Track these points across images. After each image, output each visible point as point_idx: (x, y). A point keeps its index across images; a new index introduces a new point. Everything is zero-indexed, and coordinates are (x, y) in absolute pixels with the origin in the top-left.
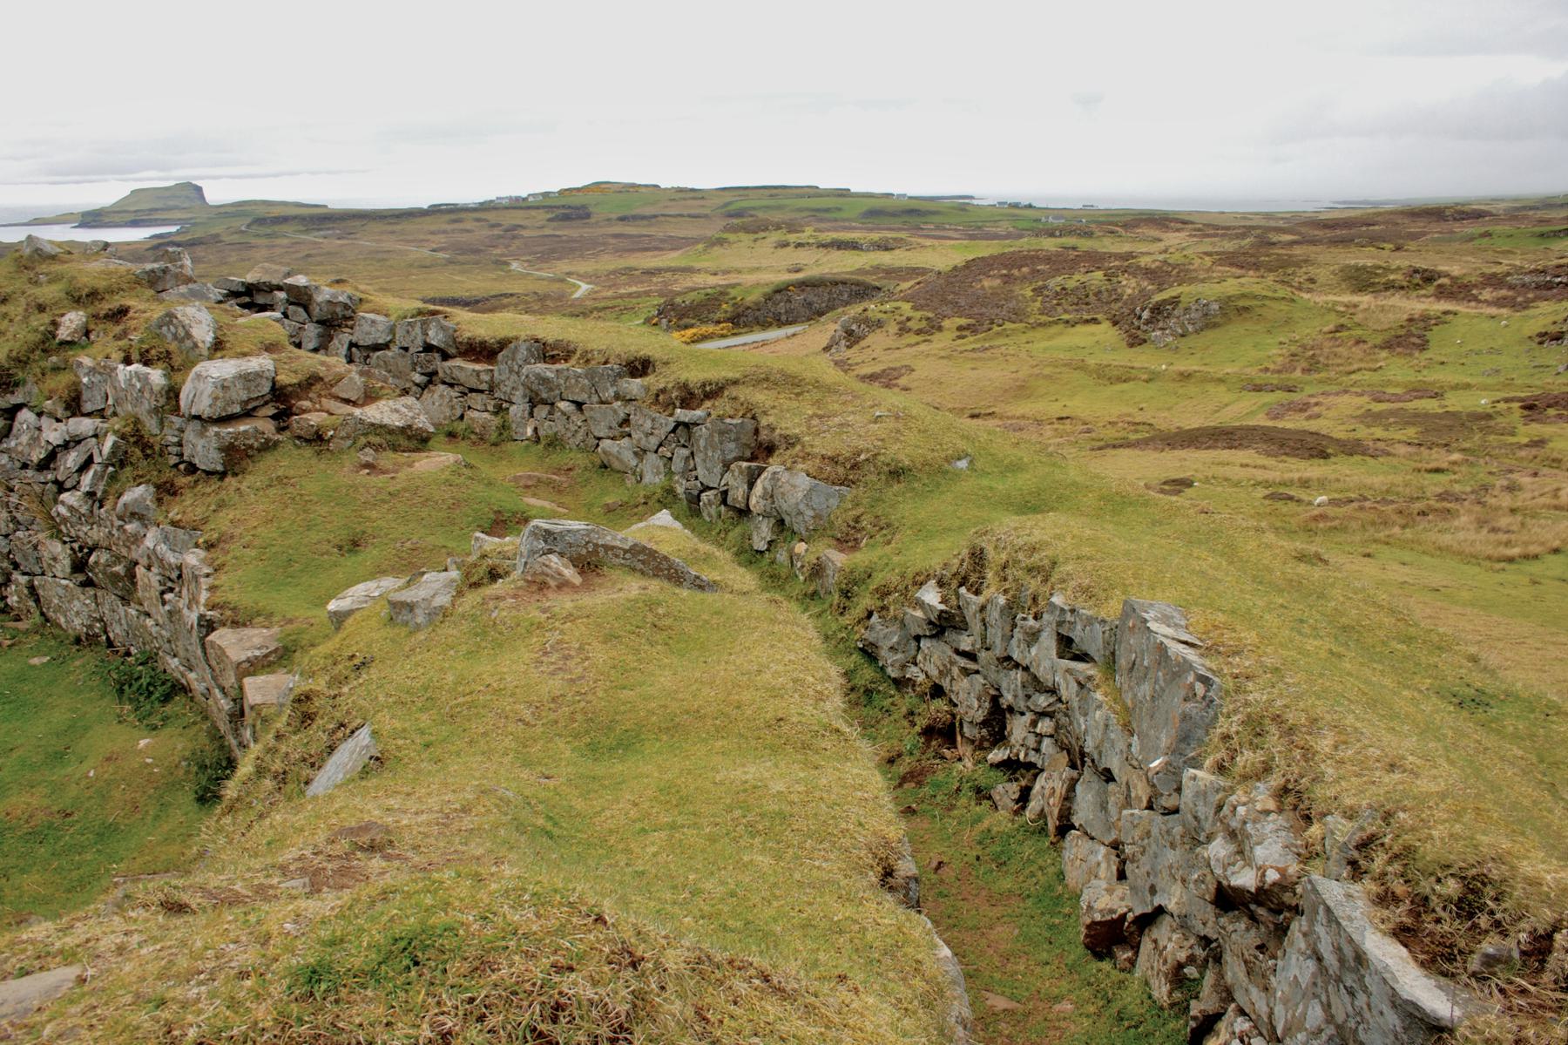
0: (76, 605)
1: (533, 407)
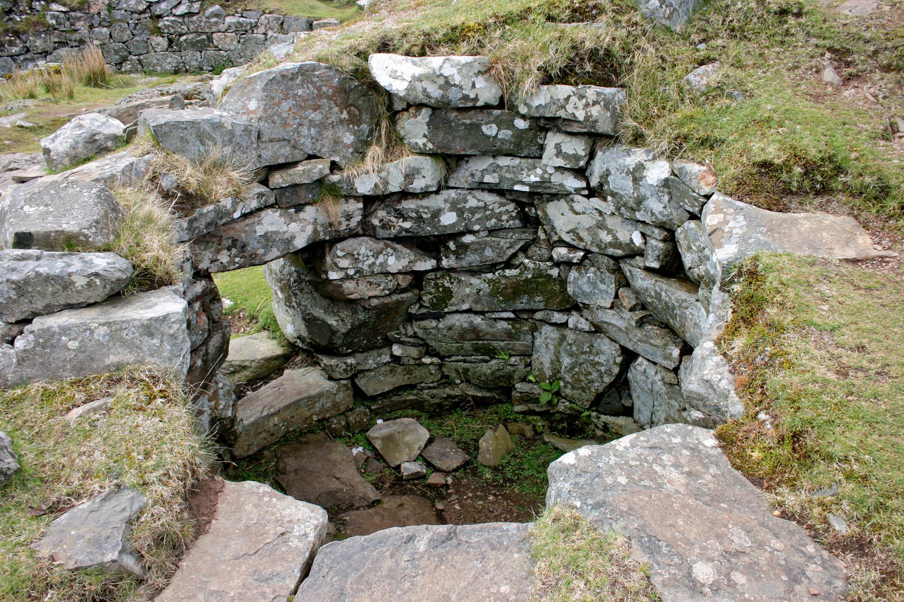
0: (169, 59)
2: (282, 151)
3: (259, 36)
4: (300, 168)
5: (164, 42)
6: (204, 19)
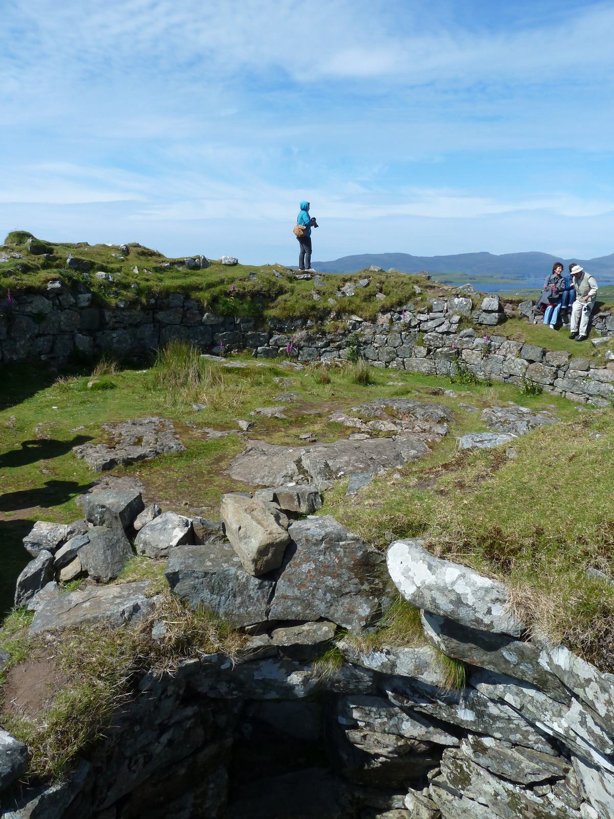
0: (425, 365)
2: (294, 609)
3: (499, 356)
4: (306, 627)
5: (424, 351)
6: (458, 338)
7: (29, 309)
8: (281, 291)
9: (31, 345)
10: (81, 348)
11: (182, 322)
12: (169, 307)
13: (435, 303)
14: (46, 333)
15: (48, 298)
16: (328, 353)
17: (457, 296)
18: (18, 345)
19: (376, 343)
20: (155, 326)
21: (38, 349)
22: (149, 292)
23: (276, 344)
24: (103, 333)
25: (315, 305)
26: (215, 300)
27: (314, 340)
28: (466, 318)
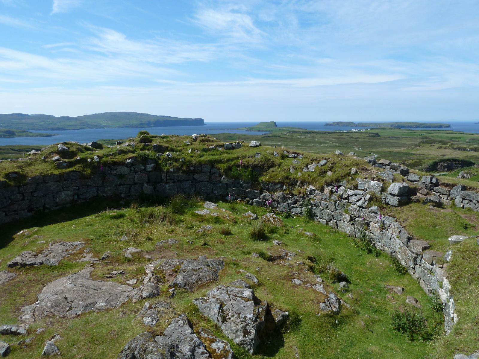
0: (349, 228)
1: (463, 199)
5: (348, 218)
7: (115, 172)
8: (273, 165)
9: (115, 190)
10: (146, 192)
11: (209, 180)
12: (201, 172)
13: (360, 183)
14: (126, 183)
15: (127, 167)
16: (295, 208)
17: (373, 179)
18: (106, 189)
19: (321, 206)
20: (192, 182)
21: (120, 192)
22: (189, 163)
23: (264, 198)
24: (160, 185)
25: (288, 176)
26: (229, 169)
27: (287, 198)
28: (376, 198)
